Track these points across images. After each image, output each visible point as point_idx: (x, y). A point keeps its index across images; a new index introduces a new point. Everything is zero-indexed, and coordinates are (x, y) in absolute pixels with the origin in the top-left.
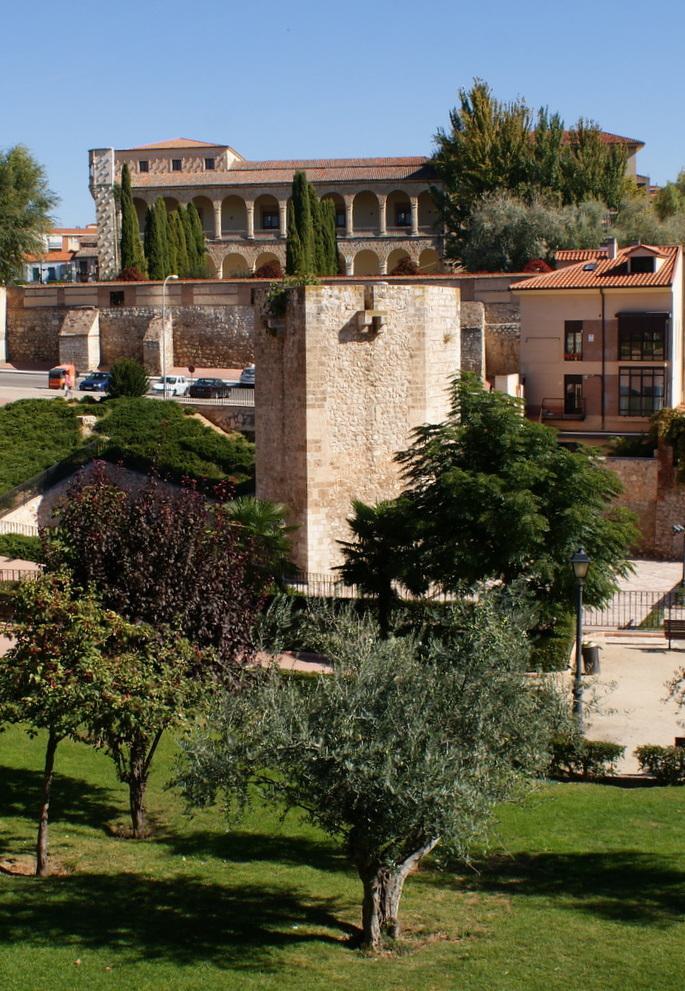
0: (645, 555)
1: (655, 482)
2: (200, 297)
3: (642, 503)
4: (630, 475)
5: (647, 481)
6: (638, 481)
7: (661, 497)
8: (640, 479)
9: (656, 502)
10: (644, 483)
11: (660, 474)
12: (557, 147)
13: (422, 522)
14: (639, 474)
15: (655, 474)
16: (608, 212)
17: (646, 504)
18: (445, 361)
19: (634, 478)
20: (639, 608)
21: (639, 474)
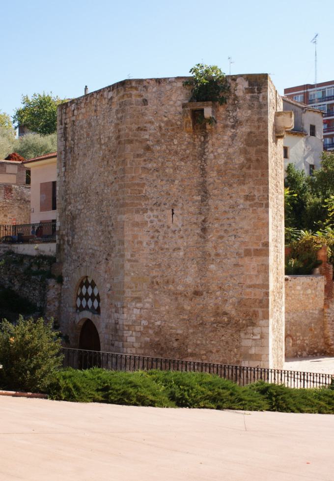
0: (318, 354)
1: (323, 294)
2: (278, 108)
3: (314, 312)
4: (306, 289)
5: (317, 293)
6: (312, 293)
7: (326, 305)
8: (313, 292)
9: (323, 310)
10: (316, 296)
11: (326, 286)
12: (27, 343)
13: (316, 180)
14: (313, 288)
15: (323, 288)
16: (330, 190)
17: (317, 312)
18: (282, 143)
19: (309, 291)
20: (312, 383)
21: (313, 288)
